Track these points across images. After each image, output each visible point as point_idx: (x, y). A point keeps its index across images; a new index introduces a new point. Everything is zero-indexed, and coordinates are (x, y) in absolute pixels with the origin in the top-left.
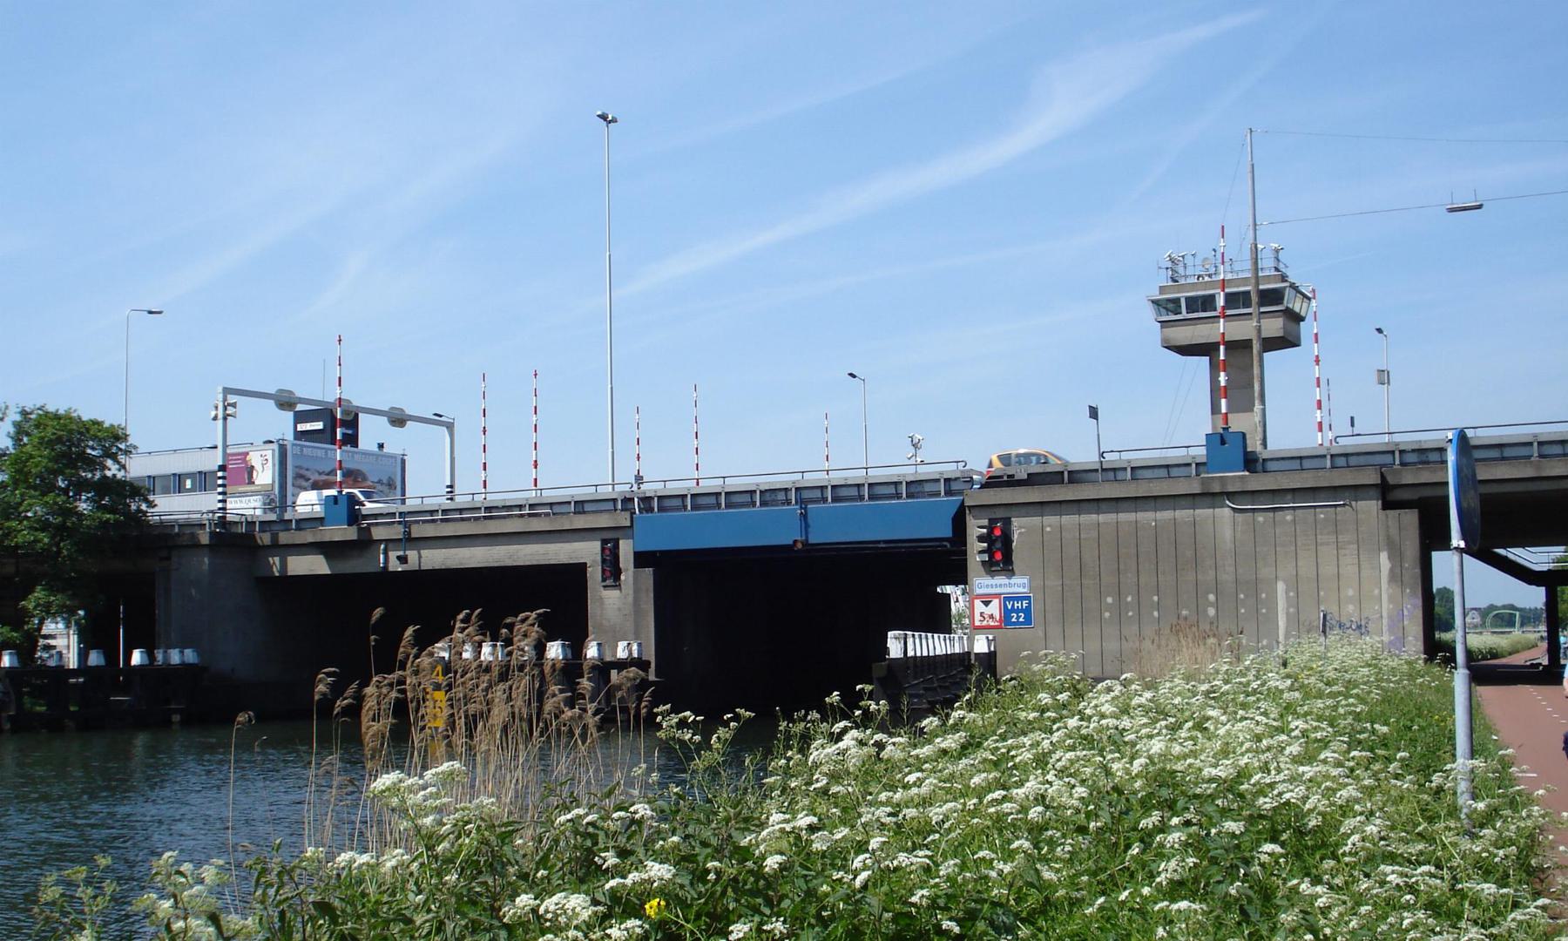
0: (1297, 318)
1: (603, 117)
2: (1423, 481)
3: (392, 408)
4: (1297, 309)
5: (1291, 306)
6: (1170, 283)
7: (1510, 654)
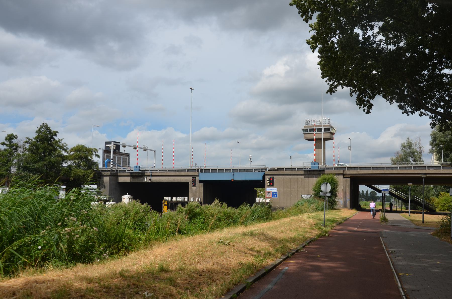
0: (333, 134)
1: (191, 89)
2: (351, 173)
3: (123, 143)
4: (333, 132)
5: (331, 131)
6: (306, 125)
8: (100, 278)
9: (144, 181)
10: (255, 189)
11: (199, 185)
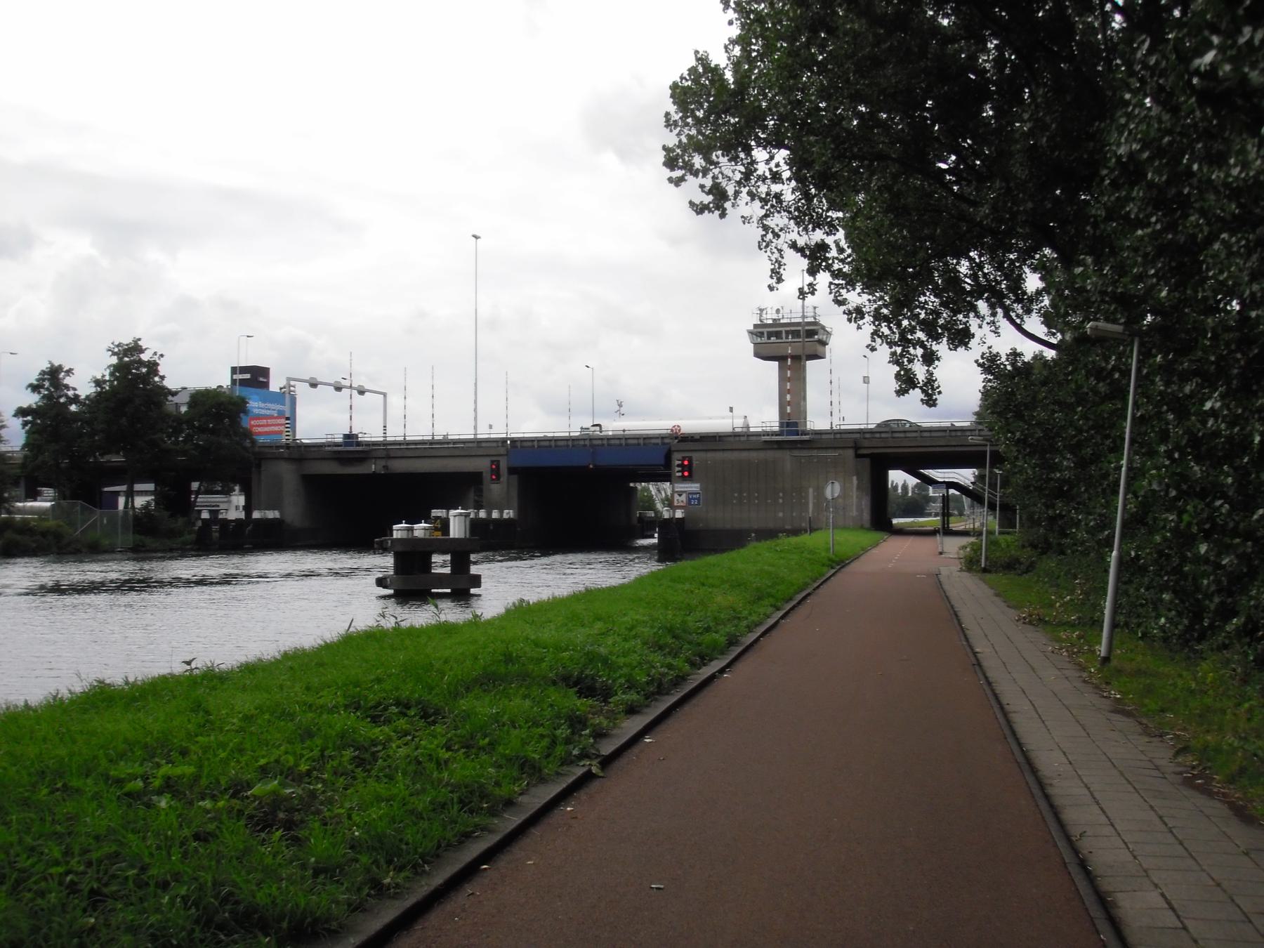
1: (474, 236)
4: (824, 339)
7: (289, 575)
8: (170, 765)
9: (371, 472)
10: (632, 485)
11: (508, 480)
